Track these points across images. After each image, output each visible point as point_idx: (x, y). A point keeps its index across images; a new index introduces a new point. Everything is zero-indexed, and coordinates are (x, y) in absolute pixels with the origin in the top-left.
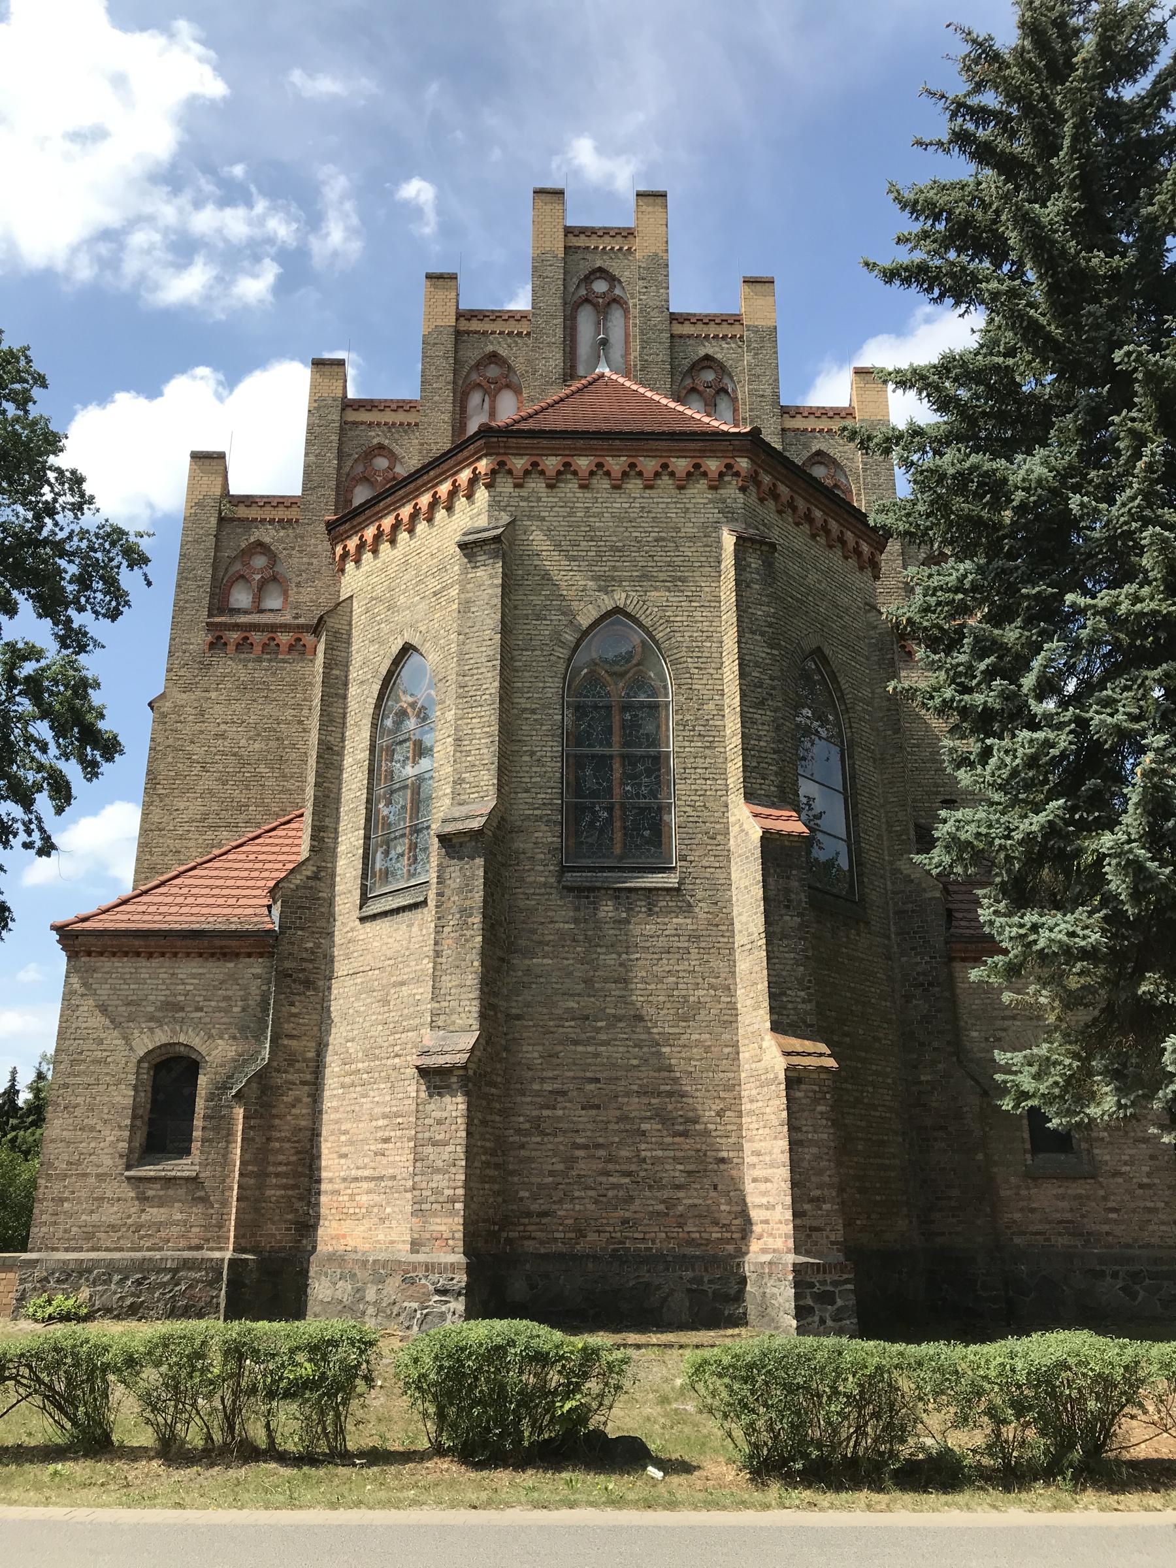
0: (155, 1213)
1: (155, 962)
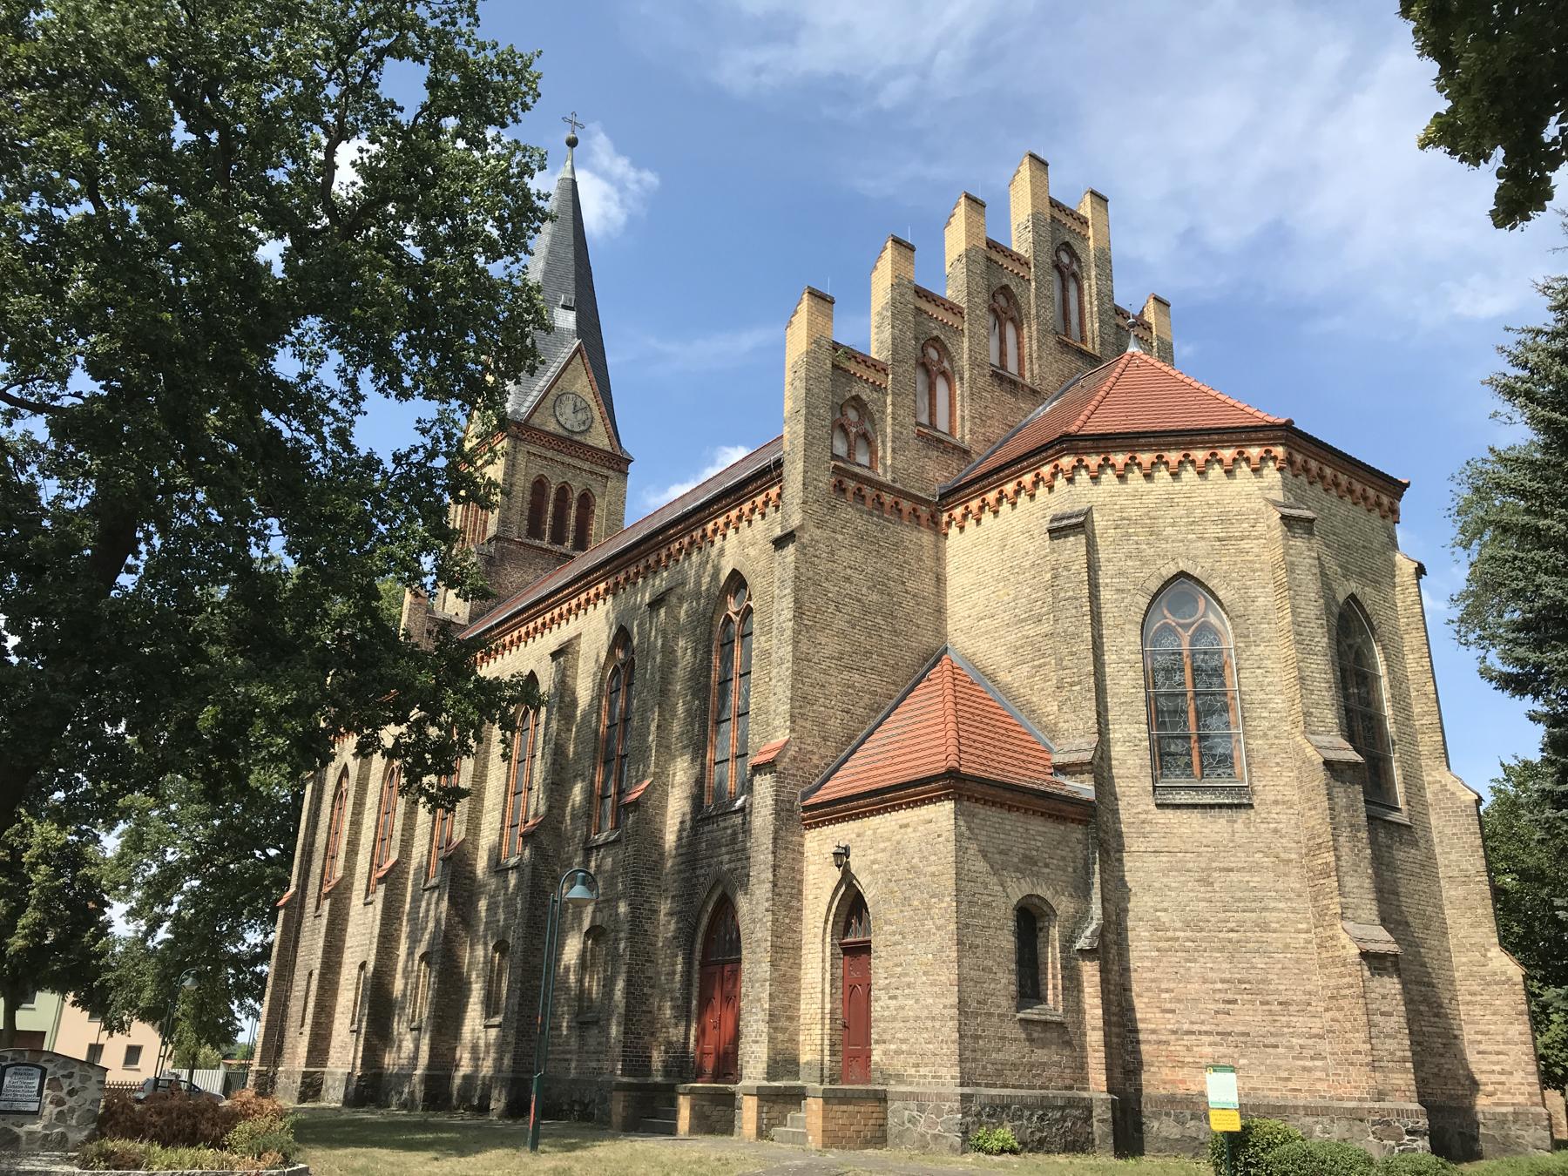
0: (1040, 1055)
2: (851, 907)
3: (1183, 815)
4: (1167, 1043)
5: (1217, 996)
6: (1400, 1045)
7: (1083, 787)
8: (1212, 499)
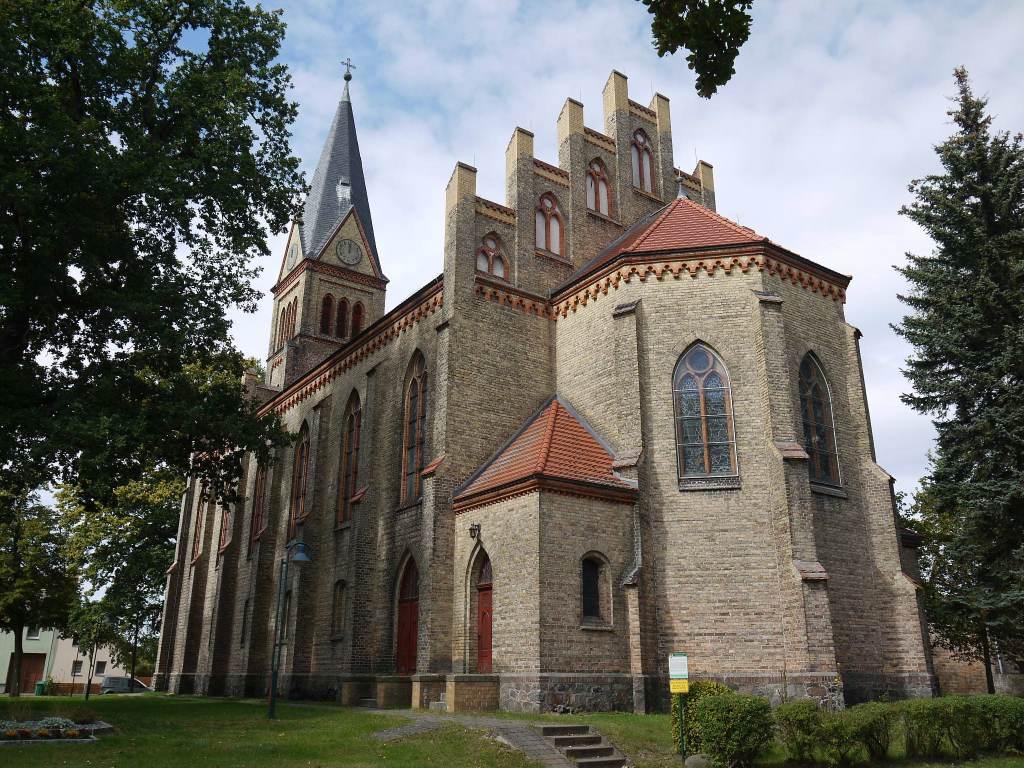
1: (581, 501)
2: (482, 561)
3: (696, 496)
4: (685, 641)
5: (716, 611)
6: (826, 636)
7: (631, 481)
8: (717, 292)
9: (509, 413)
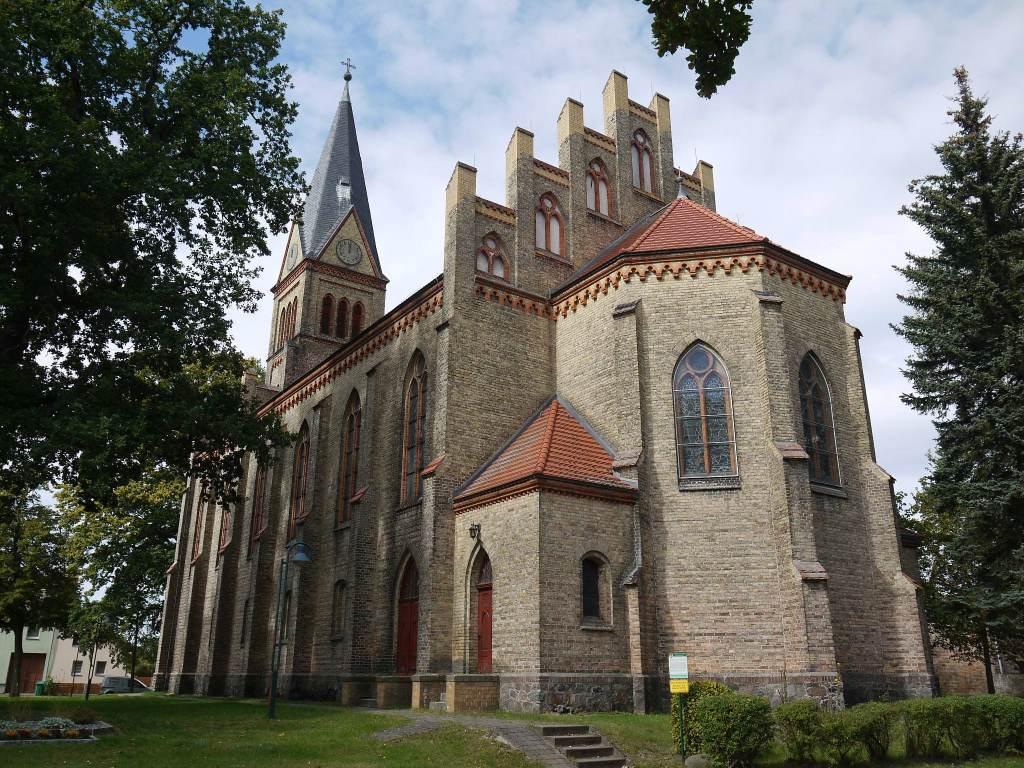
1: (581, 501)
2: (482, 561)
3: (696, 496)
4: (685, 641)
5: (716, 611)
6: (826, 636)
7: (631, 481)
8: (717, 292)
9: (509, 413)
